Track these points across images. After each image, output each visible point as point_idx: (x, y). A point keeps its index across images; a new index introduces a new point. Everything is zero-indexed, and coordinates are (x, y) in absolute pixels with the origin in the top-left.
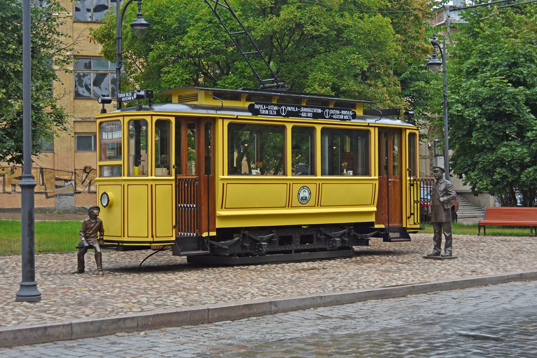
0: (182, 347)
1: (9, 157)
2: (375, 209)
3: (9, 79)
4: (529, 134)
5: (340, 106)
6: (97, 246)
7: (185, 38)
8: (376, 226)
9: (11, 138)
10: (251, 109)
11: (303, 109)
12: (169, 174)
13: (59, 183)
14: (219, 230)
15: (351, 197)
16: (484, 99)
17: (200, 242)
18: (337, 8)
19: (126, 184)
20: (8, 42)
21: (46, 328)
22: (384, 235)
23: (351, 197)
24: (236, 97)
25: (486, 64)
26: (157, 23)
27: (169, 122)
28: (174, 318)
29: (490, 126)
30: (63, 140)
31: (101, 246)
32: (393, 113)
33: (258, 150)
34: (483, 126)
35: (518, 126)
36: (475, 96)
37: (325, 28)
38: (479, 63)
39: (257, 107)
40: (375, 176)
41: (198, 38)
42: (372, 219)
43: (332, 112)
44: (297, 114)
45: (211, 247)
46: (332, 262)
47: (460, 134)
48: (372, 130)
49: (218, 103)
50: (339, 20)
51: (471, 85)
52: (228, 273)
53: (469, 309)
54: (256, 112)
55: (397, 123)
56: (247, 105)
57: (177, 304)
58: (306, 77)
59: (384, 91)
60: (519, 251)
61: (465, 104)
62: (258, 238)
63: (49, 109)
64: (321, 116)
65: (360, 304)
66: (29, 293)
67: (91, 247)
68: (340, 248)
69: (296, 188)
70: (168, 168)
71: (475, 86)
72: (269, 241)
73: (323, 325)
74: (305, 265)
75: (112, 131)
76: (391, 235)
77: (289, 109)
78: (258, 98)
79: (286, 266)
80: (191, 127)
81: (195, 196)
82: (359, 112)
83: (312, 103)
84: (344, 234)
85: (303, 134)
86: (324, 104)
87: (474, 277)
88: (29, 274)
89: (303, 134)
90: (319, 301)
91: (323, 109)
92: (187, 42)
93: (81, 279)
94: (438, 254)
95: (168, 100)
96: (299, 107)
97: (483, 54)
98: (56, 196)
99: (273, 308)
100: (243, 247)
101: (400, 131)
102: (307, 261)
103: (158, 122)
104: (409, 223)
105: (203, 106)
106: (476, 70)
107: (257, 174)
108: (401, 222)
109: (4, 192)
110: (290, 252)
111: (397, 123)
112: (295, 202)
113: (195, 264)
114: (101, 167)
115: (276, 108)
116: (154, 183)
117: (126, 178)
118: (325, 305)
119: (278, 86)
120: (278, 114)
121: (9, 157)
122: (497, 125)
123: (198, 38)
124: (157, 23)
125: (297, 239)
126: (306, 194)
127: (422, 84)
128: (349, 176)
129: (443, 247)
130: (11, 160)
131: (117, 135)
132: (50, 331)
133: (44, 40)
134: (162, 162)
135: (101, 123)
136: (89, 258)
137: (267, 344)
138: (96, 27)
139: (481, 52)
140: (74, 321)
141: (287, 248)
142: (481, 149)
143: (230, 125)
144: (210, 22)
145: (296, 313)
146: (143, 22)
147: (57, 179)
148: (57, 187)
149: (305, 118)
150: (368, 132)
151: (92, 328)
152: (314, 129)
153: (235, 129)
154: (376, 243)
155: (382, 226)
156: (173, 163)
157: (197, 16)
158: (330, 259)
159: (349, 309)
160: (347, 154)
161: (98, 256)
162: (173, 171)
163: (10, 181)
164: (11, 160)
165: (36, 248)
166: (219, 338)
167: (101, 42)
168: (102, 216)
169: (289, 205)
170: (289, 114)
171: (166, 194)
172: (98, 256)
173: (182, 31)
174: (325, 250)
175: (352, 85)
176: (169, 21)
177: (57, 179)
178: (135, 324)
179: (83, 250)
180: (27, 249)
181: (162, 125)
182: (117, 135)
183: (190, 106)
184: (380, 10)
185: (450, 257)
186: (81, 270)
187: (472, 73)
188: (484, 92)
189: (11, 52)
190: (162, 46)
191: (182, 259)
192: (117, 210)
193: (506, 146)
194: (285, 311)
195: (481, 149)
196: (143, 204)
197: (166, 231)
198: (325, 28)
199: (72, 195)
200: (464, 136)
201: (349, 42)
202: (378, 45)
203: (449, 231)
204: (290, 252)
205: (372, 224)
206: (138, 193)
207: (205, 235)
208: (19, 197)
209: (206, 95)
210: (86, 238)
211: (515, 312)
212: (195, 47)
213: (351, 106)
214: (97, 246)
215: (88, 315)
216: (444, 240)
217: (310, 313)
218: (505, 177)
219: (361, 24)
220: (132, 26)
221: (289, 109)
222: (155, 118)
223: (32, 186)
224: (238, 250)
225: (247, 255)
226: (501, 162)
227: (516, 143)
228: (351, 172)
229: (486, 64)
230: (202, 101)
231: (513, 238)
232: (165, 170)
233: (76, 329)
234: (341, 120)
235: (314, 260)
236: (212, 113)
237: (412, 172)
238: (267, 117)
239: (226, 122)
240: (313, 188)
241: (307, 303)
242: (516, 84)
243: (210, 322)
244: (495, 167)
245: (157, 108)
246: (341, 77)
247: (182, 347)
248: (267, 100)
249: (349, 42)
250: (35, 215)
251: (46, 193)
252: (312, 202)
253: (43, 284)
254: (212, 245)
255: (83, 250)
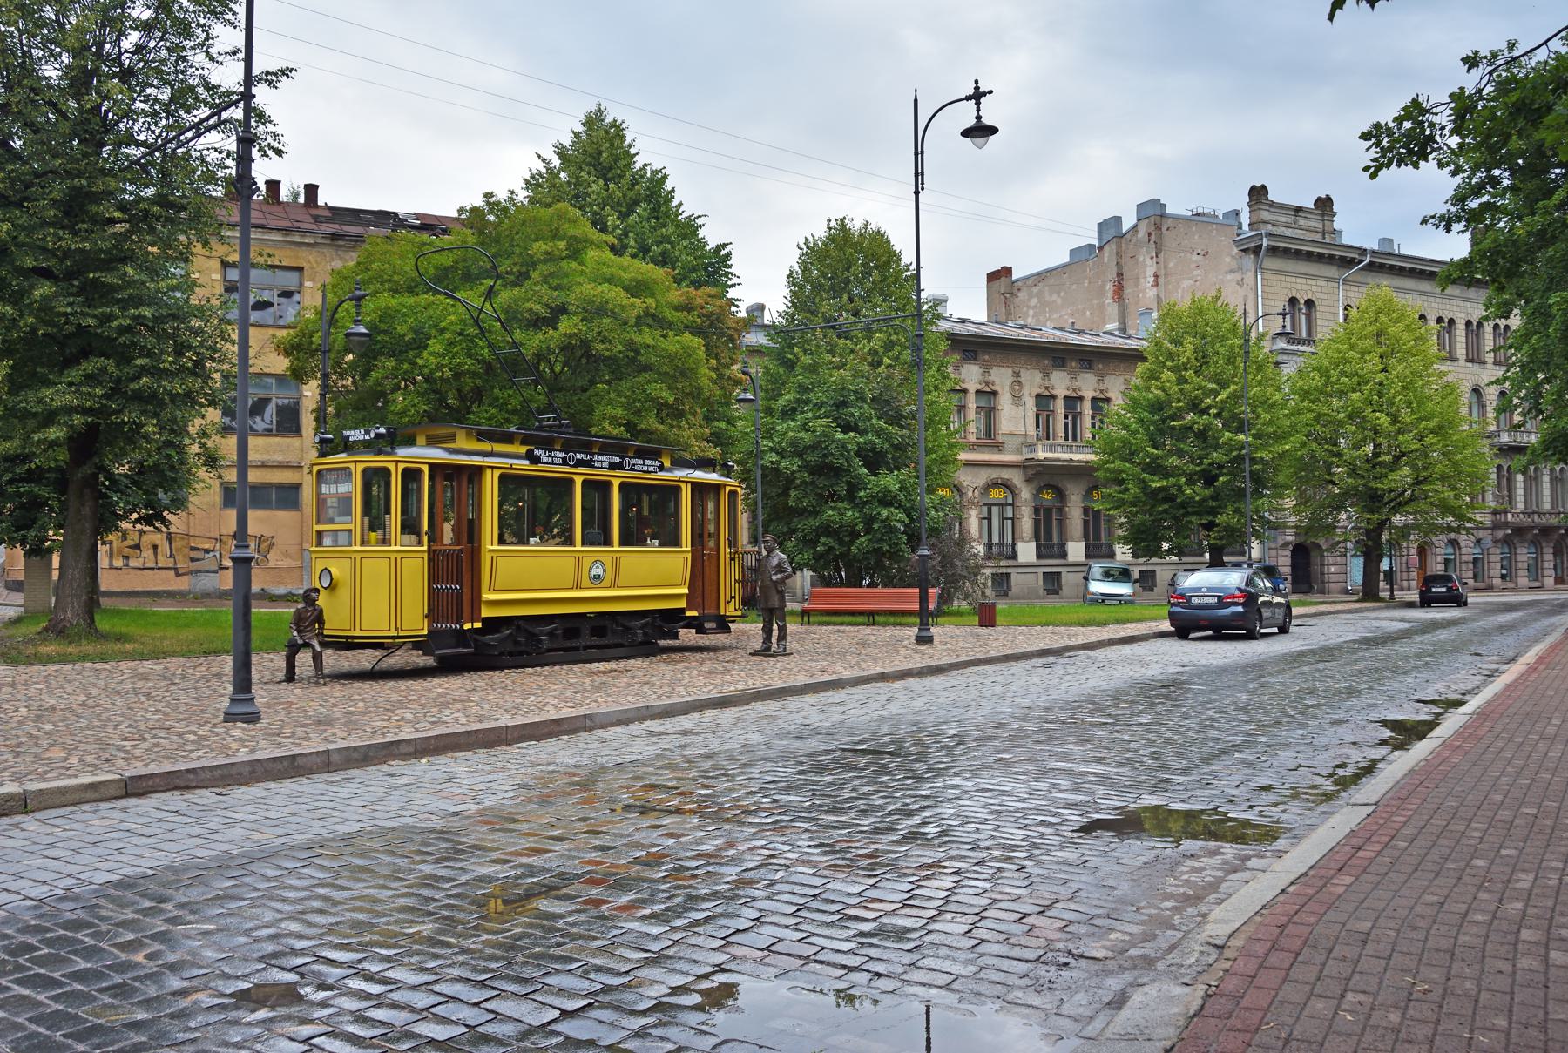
0: (490, 777)
1: (135, 516)
2: (686, 591)
3: (162, 405)
4: (862, 494)
5: (644, 454)
6: (315, 643)
7: (425, 354)
8: (688, 614)
9: (140, 488)
10: (532, 458)
11: (597, 457)
12: (420, 543)
13: (195, 555)
14: (485, 621)
15: (653, 575)
16: (806, 448)
17: (461, 637)
18: (632, 321)
19: (358, 556)
20: (162, 352)
21: (294, 756)
22: (697, 625)
23: (653, 575)
24: (508, 438)
25: (807, 402)
26: (384, 332)
27: (420, 471)
28: (462, 740)
29: (812, 483)
30: (205, 492)
31: (323, 645)
32: (705, 464)
33: (536, 512)
34: (804, 482)
35: (848, 483)
36: (794, 443)
37: (620, 347)
38: (797, 401)
39: (537, 452)
40: (686, 547)
41: (443, 355)
42: (682, 604)
43: (633, 461)
44: (589, 464)
45: (469, 641)
46: (632, 661)
47: (774, 492)
48: (683, 486)
49: (486, 447)
50: (637, 338)
51: (788, 429)
52: (498, 676)
53: (837, 718)
54: (535, 460)
55: (713, 477)
56: (523, 450)
57: (456, 722)
58: (591, 412)
59: (691, 435)
60: (863, 644)
61: (781, 454)
62: (537, 630)
63: (195, 448)
64: (619, 466)
65: (696, 715)
66: (242, 710)
67: (307, 645)
68: (641, 644)
69: (587, 562)
70: (419, 535)
71: (794, 430)
72: (551, 634)
73: (664, 743)
74: (601, 666)
75: (336, 482)
76: (707, 625)
77: (579, 456)
78: (539, 441)
79: (577, 667)
80: (448, 478)
81: (454, 573)
82: (667, 464)
83: (606, 450)
84: (646, 625)
85: (599, 489)
86: (622, 451)
87: (826, 678)
88: (243, 683)
89: (599, 489)
90: (645, 712)
91: (622, 458)
92: (428, 359)
93: (295, 692)
94: (768, 649)
95: (410, 441)
96: (592, 454)
97: (803, 389)
98: (191, 573)
99: (588, 723)
100: (516, 643)
101: (716, 488)
102: (599, 661)
103: (405, 470)
104: (729, 610)
105: (463, 450)
106: (794, 410)
107: (537, 544)
108: (718, 607)
109: (112, 567)
110: (576, 649)
111: (713, 477)
112: (586, 581)
113: (448, 667)
114: (319, 533)
115: (562, 455)
116: (399, 556)
117: (358, 548)
118: (653, 718)
119: (561, 426)
120: (565, 463)
121: (135, 516)
122: (822, 482)
123: (443, 355)
124: (384, 332)
125: (586, 631)
126: (600, 571)
127: (723, 425)
128: (654, 547)
129: (774, 640)
130: (137, 521)
131: (344, 488)
132: (300, 761)
133: (215, 351)
134: (410, 527)
135: (319, 472)
136: (304, 659)
137: (603, 770)
138: (282, 333)
139: (800, 385)
140: (331, 747)
141: (574, 643)
142: (801, 513)
143: (502, 477)
144: (460, 334)
145: (618, 729)
146: (362, 329)
147: (193, 549)
148: (192, 560)
149: (599, 472)
150: (678, 489)
151: (356, 755)
152: (572, 481)
153: (509, 482)
154: (687, 636)
155: (695, 614)
156: (426, 528)
157: (443, 325)
158: (628, 658)
159: (687, 721)
160: (650, 517)
161: (317, 658)
162: (425, 539)
163: (120, 551)
164: (137, 521)
165: (254, 644)
166: (534, 765)
167: (287, 354)
168: (321, 602)
169: (577, 586)
170: (580, 463)
171: (415, 569)
172: (317, 658)
173: (420, 344)
174: (622, 646)
175: (651, 422)
176: (401, 329)
177: (193, 549)
178: (412, 749)
179: (293, 649)
180: (242, 648)
181: (411, 476)
182: (344, 488)
183: (447, 450)
184: (686, 327)
185: (784, 653)
186: (290, 677)
187: (789, 413)
188: (806, 437)
189: (166, 365)
190: (391, 364)
191: (427, 661)
192: (344, 593)
193: (832, 508)
194: (604, 726)
195: (801, 513)
196: (383, 588)
197: (416, 623)
198: (620, 347)
199: (215, 572)
200: (778, 495)
201: (647, 368)
202: (686, 373)
203: (783, 620)
204: (576, 649)
205: (682, 610)
206: (376, 570)
207: (467, 626)
208: (229, 574)
209: (469, 435)
210: (299, 632)
211: (896, 719)
212: (440, 367)
213: (655, 454)
214: (315, 643)
215: (341, 740)
216: (775, 633)
217: (635, 728)
218: (831, 549)
219: (664, 344)
220: (348, 335)
221: (579, 456)
222: (401, 466)
223: (249, 560)
224: (509, 647)
225: (521, 653)
226: (827, 530)
227: (845, 505)
228: (656, 542)
229: (807, 402)
230: (462, 442)
231: (848, 628)
232: (413, 537)
233: (335, 758)
234: (645, 472)
235: (607, 660)
236: (476, 461)
237: (733, 542)
238: (551, 465)
239: (497, 473)
240: (608, 562)
241: (629, 715)
242: (846, 429)
243: (508, 744)
244: (818, 536)
245: (404, 452)
246: (638, 412)
247: (490, 777)
248: (548, 445)
249: (647, 368)
250: (253, 602)
251: (176, 569)
252: (607, 582)
253: (261, 697)
254: (476, 641)
255: (293, 649)
